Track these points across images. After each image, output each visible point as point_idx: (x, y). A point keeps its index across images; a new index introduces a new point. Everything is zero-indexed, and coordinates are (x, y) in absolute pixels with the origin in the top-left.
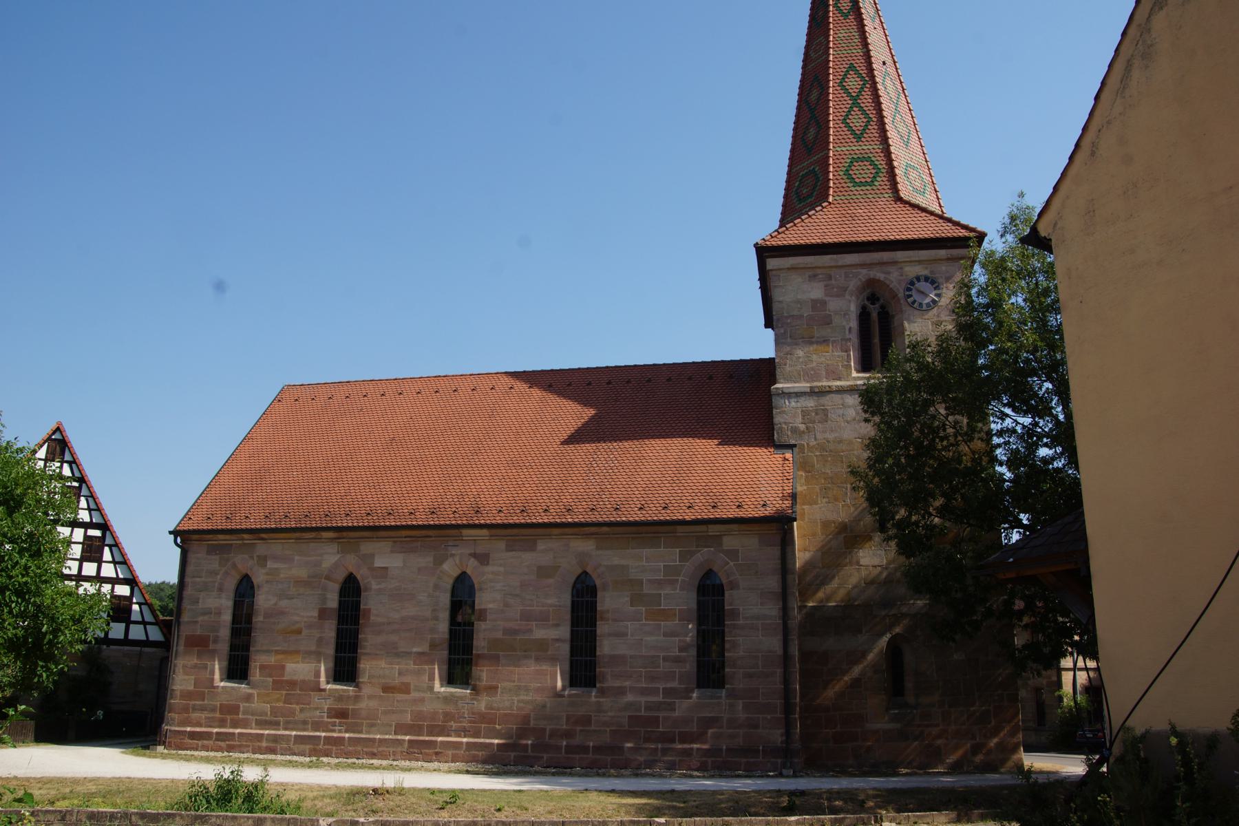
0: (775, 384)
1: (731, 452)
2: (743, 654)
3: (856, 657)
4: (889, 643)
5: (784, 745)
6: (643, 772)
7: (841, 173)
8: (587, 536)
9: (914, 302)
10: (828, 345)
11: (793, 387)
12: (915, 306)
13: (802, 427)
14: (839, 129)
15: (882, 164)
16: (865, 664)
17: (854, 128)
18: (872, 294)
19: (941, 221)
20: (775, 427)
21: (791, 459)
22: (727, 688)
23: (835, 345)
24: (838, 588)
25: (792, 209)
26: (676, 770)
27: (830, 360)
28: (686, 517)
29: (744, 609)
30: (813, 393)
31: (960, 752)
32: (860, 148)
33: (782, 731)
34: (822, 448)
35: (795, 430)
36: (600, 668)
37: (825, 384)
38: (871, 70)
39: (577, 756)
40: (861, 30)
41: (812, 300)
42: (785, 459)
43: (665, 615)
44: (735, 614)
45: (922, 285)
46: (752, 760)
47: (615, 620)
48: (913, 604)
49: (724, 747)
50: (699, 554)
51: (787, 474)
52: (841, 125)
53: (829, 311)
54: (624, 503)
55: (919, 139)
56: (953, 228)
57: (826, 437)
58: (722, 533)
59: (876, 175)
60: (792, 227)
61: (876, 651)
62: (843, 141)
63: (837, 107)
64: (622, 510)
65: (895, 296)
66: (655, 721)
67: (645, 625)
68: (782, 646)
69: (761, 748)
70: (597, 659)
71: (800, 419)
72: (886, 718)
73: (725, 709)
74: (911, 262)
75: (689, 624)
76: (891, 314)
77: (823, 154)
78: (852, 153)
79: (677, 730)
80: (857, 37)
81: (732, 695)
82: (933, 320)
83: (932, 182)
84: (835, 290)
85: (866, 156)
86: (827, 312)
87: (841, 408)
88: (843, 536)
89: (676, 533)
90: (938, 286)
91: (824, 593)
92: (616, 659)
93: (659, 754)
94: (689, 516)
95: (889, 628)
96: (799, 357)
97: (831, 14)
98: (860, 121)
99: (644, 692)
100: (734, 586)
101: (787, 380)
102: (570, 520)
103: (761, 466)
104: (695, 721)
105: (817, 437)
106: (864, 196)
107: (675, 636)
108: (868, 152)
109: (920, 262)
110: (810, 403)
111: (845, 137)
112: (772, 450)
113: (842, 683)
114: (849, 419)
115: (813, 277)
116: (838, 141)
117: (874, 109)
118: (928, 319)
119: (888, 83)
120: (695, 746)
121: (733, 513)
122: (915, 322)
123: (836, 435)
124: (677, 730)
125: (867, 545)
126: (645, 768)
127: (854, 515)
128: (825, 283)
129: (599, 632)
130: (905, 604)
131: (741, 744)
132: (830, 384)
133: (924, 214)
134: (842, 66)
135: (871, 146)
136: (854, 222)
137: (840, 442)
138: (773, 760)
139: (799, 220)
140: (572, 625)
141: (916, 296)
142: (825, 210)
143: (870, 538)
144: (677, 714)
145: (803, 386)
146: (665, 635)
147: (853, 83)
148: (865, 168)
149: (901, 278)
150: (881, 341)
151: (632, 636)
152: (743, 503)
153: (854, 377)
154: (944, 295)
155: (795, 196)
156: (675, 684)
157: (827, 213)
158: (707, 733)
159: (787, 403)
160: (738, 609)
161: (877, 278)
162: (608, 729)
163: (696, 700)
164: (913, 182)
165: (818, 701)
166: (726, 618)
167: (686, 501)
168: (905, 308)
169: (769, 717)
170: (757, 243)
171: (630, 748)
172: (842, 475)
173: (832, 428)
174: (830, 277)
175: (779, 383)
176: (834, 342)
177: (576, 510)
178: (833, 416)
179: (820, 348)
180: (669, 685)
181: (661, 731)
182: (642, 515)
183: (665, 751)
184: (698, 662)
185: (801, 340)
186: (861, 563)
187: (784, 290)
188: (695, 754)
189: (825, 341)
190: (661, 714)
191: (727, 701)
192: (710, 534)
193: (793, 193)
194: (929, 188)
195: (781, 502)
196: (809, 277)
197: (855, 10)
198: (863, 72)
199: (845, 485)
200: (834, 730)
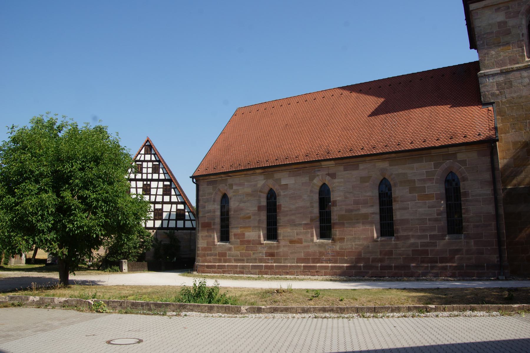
10: (510, 46)
13: (497, 92)
20: (482, 94)
22: (465, 234)
28: (436, 145)
29: (471, 191)
30: (502, 73)
35: (493, 95)
37: (509, 67)
39: (386, 271)
42: (489, 110)
43: (428, 197)
44: (466, 194)
49: (465, 265)
50: (444, 164)
51: (490, 118)
54: (402, 141)
57: (512, 96)
58: (457, 152)
64: (401, 145)
66: (426, 252)
69: (485, 265)
70: (394, 222)
71: (496, 88)
73: (464, 245)
75: (441, 201)
86: (508, 28)
87: (520, 79)
88: (526, 149)
92: (404, 222)
93: (429, 269)
94: (438, 144)
96: (493, 55)
99: (419, 237)
100: (465, 179)
101: (487, 67)
104: (448, 251)
105: (507, 96)
110: (501, 79)
114: (525, 84)
115: (497, 10)
123: (518, 94)
124: (438, 257)
126: (422, 277)
129: (394, 208)
140: (380, 205)
144: (438, 248)
145: (496, 70)
146: (429, 207)
156: (436, 233)
159: (488, 81)
160: (468, 191)
162: (402, 257)
166: (462, 196)
167: (435, 137)
169: (489, 248)
173: (515, 91)
174: (508, 8)
175: (482, 70)
176: (513, 43)
178: (515, 84)
180: (432, 233)
183: (432, 268)
187: (481, 20)
188: (448, 268)
189: (507, 44)
190: (429, 249)
192: (450, 153)
195: (488, 132)
196: (496, 10)
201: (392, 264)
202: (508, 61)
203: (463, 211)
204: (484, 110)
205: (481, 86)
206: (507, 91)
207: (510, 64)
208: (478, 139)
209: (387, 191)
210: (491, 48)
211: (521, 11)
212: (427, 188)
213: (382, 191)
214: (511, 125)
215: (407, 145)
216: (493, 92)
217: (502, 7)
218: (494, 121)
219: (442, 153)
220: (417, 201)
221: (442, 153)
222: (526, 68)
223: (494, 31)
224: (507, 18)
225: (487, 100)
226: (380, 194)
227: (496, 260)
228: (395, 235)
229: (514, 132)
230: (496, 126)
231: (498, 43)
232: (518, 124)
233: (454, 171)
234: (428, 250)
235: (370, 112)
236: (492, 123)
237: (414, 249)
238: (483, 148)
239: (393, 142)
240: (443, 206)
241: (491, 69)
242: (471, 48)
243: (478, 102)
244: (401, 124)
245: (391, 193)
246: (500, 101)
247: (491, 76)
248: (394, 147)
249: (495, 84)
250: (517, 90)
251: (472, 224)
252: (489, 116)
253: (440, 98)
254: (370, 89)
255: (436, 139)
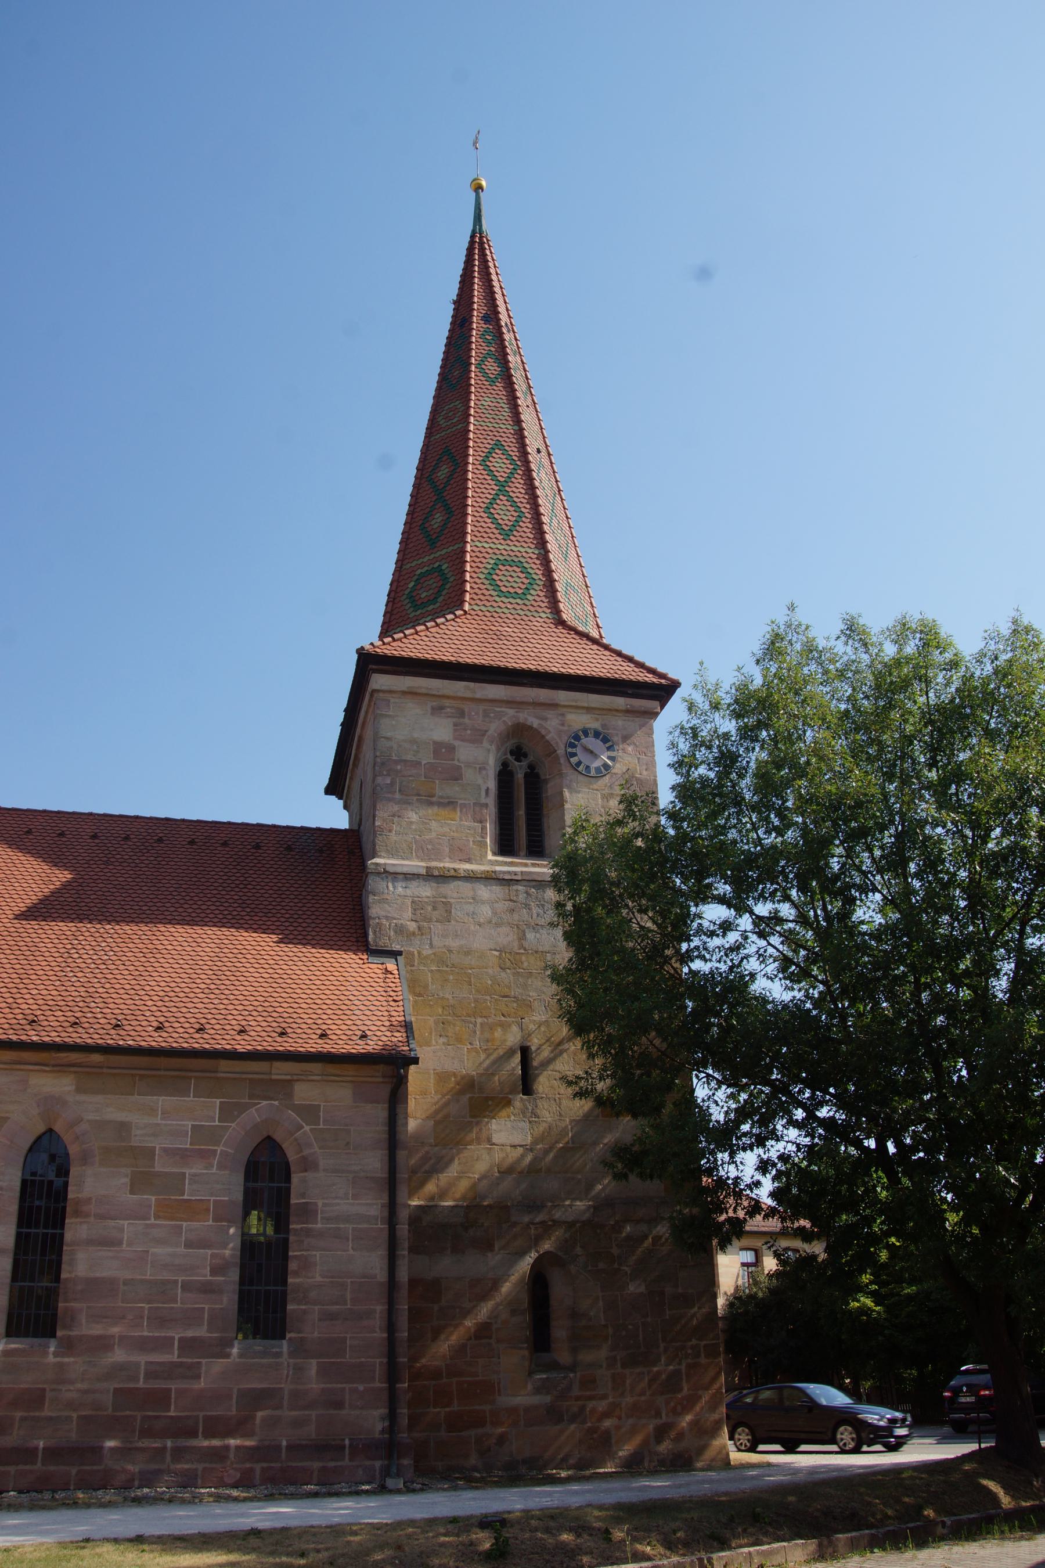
0: (374, 858)
1: (300, 954)
2: (322, 1280)
3: (482, 1289)
4: (533, 1266)
5: (386, 1436)
6: (139, 1493)
7: (482, 576)
8: (61, 1068)
9: (579, 763)
10: (455, 809)
11: (402, 865)
12: (580, 769)
13: (412, 926)
14: (479, 519)
15: (538, 574)
16: (498, 1300)
17: (500, 521)
18: (517, 747)
19: (618, 658)
20: (371, 922)
21: (396, 972)
22: (290, 1339)
23: (464, 810)
24: (459, 1178)
25: (392, 624)
26: (196, 1488)
27: (457, 832)
28: (238, 1047)
29: (325, 1205)
30: (430, 876)
31: (637, 1440)
32: (508, 548)
33: (384, 1411)
34: (441, 961)
35: (400, 930)
36: (66, 1301)
37: (448, 865)
38: (524, 454)
39: (12, 1469)
40: (512, 402)
41: (435, 743)
42: (387, 971)
43: (192, 1210)
44: (308, 1212)
45: (590, 742)
46: (332, 1464)
47: (103, 1217)
48: (570, 1206)
49: (284, 1443)
50: (253, 1110)
51: (392, 994)
52: (482, 514)
53: (458, 760)
54: (128, 1017)
55: (578, 556)
56: (636, 669)
57: (447, 944)
58: (295, 1077)
59: (529, 586)
60: (412, 634)
61: (513, 1279)
62: (485, 535)
63: (478, 490)
64: (126, 1028)
65: (551, 752)
66: (162, 1398)
67: (153, 1226)
68: (386, 1267)
69: (347, 1442)
70: (61, 1286)
71: (409, 914)
72: (530, 1387)
73: (287, 1376)
74: (577, 707)
75: (229, 1227)
76: (543, 777)
77: (455, 547)
78: (498, 552)
79: (201, 1414)
80: (506, 410)
81: (300, 1349)
82: (604, 792)
83: (594, 614)
84: (469, 732)
85: (516, 560)
86: (456, 762)
87: (471, 903)
88: (468, 1096)
89: (216, 1072)
90: (612, 746)
91: (438, 1186)
92: (96, 1287)
93: (168, 1458)
94: (242, 1045)
95: (537, 1240)
96: (411, 823)
97: (473, 375)
98: (508, 513)
99: (144, 1345)
100: (308, 1165)
101: (393, 853)
102: (35, 1038)
103: (350, 979)
104: (235, 1396)
105: (435, 943)
106: (513, 612)
107: (204, 1248)
108: (519, 555)
109: (589, 710)
110: (425, 891)
111: (488, 530)
112: (365, 957)
113: (461, 1331)
114: (482, 920)
115: (437, 710)
116: (478, 534)
117: (527, 503)
118: (597, 790)
119: (543, 475)
120: (233, 1442)
121: (314, 1045)
122: (579, 792)
123: (463, 942)
124: (201, 1414)
125: (504, 1113)
126: (140, 1487)
127: (485, 1065)
128: (454, 720)
129: (68, 1236)
130: (558, 1205)
131: (314, 1436)
132: (456, 866)
133: (595, 647)
134: (485, 441)
135: (525, 550)
136: (500, 642)
137: (468, 953)
138: (368, 1463)
139: (423, 627)
140: (20, 1224)
141: (582, 756)
142: (458, 620)
143: (508, 1103)
144: (202, 1384)
145: (415, 864)
146: (189, 1245)
147: (500, 465)
148: (514, 574)
149: (561, 728)
150: (527, 814)
151: (130, 1244)
152: (329, 1032)
153: (490, 860)
154: (620, 759)
155: (448, 576)
156: (201, 1332)
157: (461, 624)
158: (254, 1417)
159: (391, 888)
160: (316, 1204)
161: (529, 723)
162: (75, 1415)
163: (238, 1360)
164: (574, 607)
165: (424, 1361)
166: (292, 1219)
167: (234, 1022)
168: (566, 770)
169: (361, 1388)
170: (362, 648)
171: (111, 1449)
172: (470, 1004)
173: (456, 932)
174: (462, 714)
175: (380, 857)
176: (463, 806)
177: (46, 1023)
178: (459, 914)
179: (444, 812)
180: (190, 1334)
181: (172, 1417)
182: (161, 1039)
183: (179, 1453)
184: (241, 1292)
185: (415, 798)
186: (494, 1141)
187: (394, 722)
188: (232, 1456)
189: (450, 804)
190: (173, 1386)
191: (291, 1360)
192: (274, 1077)
193: (405, 597)
194: (590, 619)
195: (388, 1034)
196: (433, 708)
197: (504, 377)
198: (515, 454)
199: (473, 1020)
200: (447, 1409)
201: (35, 1442)
202: (447, 850)
203: (292, 1266)
204: (374, 967)
205: (371, 898)
206: (437, 928)
207: (450, 858)
208: (359, 1047)
209: (52, 1176)
210: (409, 803)
211: (490, 733)
212: (190, 1179)
213: (34, 1174)
214: (436, 1023)
215: (143, 1034)
216: (402, 924)
217: (449, 707)
218: (401, 1003)
219: (251, 1076)
220: (152, 1221)
221: (251, 1076)
222: (486, 878)
223: (424, 762)
224: (455, 739)
225: (384, 943)
226: (25, 1185)
227: (379, 1427)
228: (59, 1333)
229: (444, 1044)
230: (408, 1019)
231: (429, 796)
232: (454, 1025)
233: (278, 1136)
234: (170, 1390)
235: (22, 905)
236: (396, 1008)
237: (121, 1386)
238: (372, 1077)
239: (99, 1016)
240: (231, 1245)
241: (403, 859)
242: (328, 791)
243: (357, 941)
244: (127, 963)
245: (66, 1184)
246: (416, 952)
247: (401, 877)
248: (101, 1031)
249: (409, 902)
250: (461, 931)
251: (316, 1308)
252: (389, 989)
253: (248, 910)
254: (29, 832)
255: (235, 1028)
